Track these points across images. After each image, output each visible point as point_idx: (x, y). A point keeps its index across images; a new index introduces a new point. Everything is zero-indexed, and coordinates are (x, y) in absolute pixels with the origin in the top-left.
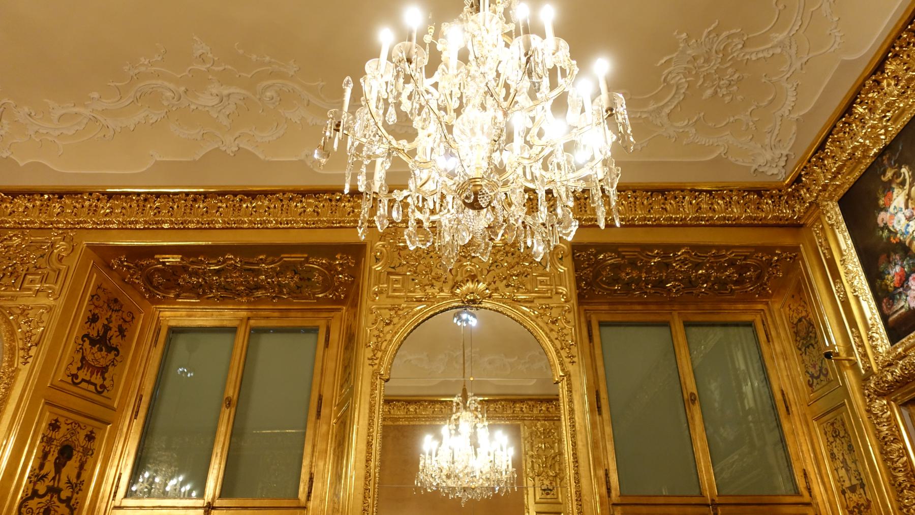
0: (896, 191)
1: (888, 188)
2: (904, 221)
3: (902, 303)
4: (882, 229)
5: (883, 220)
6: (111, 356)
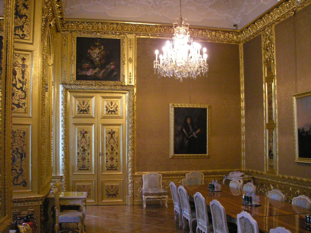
0: (97, 49)
1: (96, 46)
2: (96, 56)
3: (85, 72)
4: (88, 53)
5: (90, 52)
6: (24, 19)
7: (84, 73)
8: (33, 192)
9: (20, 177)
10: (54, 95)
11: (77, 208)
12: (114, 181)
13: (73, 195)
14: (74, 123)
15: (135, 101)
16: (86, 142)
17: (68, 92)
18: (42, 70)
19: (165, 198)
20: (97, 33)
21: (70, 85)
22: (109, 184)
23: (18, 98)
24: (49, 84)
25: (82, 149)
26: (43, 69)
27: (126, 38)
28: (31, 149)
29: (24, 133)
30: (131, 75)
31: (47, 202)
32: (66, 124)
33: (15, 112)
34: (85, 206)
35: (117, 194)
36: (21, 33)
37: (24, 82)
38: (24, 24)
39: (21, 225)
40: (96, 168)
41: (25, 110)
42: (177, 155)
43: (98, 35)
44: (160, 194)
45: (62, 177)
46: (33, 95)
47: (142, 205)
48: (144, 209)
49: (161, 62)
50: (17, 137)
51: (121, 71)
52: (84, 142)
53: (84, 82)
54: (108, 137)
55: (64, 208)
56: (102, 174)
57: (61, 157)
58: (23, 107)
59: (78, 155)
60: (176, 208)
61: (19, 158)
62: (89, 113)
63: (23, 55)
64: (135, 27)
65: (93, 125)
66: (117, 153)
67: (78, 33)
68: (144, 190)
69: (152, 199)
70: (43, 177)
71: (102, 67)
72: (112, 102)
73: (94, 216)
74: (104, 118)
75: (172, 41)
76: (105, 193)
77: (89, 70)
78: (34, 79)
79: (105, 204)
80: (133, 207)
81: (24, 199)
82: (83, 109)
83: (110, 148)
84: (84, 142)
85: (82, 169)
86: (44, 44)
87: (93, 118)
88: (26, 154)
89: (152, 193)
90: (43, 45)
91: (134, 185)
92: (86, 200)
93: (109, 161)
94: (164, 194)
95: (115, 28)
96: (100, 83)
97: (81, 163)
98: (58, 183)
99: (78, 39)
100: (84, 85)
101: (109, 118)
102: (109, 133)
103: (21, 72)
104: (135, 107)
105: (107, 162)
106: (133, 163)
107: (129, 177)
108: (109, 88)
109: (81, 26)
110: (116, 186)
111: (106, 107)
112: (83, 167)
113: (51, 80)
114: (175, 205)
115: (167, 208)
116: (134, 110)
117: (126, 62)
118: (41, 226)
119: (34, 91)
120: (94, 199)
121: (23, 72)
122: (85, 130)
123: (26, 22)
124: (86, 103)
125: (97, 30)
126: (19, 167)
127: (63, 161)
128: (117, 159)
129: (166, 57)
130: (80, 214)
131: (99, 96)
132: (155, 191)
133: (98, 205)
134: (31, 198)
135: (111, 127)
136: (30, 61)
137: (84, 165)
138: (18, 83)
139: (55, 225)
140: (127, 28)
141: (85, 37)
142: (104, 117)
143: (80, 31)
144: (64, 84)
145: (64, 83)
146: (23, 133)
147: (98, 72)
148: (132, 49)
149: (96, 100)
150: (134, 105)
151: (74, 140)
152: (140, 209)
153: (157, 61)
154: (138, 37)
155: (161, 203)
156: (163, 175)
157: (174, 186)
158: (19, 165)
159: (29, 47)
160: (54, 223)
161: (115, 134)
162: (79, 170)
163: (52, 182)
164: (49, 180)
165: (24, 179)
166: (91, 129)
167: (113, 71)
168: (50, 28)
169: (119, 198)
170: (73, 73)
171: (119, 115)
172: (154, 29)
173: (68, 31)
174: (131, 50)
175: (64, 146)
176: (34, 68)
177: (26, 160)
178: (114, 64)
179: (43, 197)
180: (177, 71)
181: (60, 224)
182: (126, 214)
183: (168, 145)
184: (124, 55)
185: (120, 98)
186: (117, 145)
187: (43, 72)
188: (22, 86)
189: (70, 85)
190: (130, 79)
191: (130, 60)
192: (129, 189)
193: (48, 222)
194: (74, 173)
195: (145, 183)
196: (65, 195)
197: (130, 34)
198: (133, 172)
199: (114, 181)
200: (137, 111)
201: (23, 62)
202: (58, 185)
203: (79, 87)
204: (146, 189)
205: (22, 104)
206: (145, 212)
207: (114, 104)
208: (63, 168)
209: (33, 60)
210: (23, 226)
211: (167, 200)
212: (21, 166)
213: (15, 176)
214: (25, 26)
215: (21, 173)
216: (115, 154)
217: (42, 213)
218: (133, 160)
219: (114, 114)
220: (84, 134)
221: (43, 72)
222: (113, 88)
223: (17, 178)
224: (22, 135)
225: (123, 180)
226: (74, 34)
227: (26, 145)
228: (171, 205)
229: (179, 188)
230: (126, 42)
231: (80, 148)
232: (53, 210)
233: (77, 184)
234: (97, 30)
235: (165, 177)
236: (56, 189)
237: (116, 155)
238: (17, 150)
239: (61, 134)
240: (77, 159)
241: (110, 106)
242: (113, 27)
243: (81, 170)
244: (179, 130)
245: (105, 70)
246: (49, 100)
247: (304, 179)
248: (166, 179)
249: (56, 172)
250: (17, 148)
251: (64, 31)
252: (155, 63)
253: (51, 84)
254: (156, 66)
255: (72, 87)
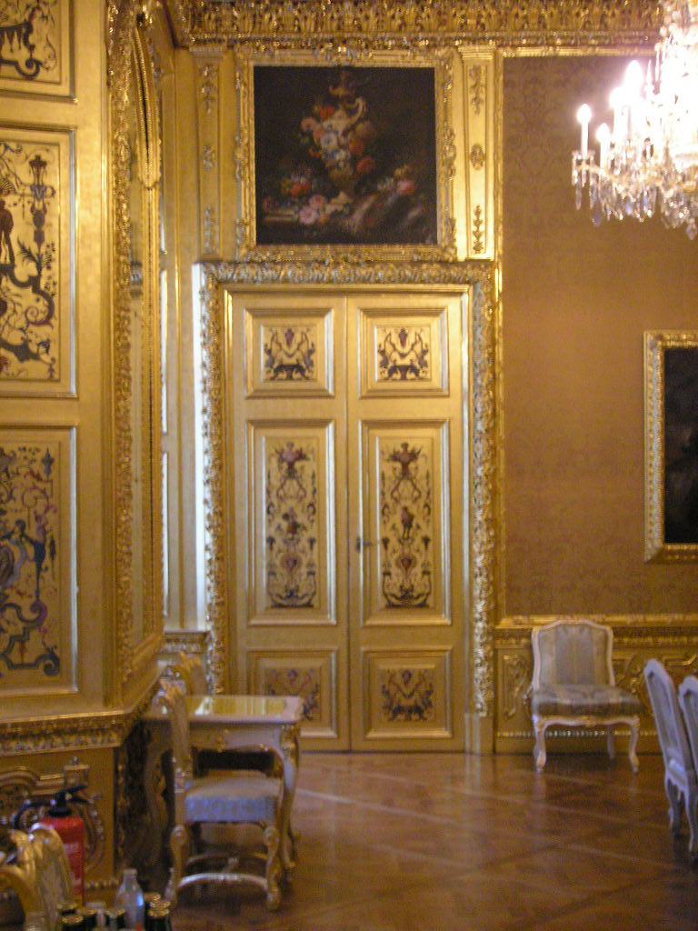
1: (333, 102)
2: (334, 143)
3: (292, 212)
4: (304, 134)
5: (308, 126)
7: (288, 214)
8: (83, 697)
9: (34, 634)
10: (171, 305)
11: (262, 762)
12: (417, 654)
13: (249, 710)
14: (252, 417)
15: (499, 323)
16: (301, 493)
17: (226, 293)
18: (113, 206)
19: (627, 726)
20: (335, 47)
21: (235, 264)
22: (395, 666)
23: (22, 323)
24: (145, 262)
25: (285, 525)
26: (119, 202)
27: (457, 59)
28: (78, 524)
29: (48, 461)
30: (482, 217)
31: (141, 741)
32: (220, 423)
33: (10, 379)
34: (296, 754)
35: (429, 704)
36: (22, 55)
37: (44, 257)
38: (32, 16)
39: (27, 833)
40: (344, 602)
41: (51, 370)
42: (676, 547)
43: (344, 55)
44: (605, 710)
45: (205, 634)
46: (81, 310)
47: (529, 755)
48: (539, 770)
49: (606, 156)
50: (21, 479)
51: (441, 200)
52: (292, 492)
53: (290, 251)
54: (389, 473)
55: (211, 763)
56: (368, 622)
57: (202, 558)
58: (44, 357)
59: (271, 548)
60: (673, 772)
61: (27, 562)
62: (314, 376)
63: (33, 147)
64: (494, 13)
65: (331, 426)
66: (426, 540)
67: (258, 48)
68: (538, 693)
69: (573, 728)
70: (127, 637)
71: (362, 186)
72: (403, 331)
73: (334, 798)
74: (373, 395)
75: (654, 64)
76: (379, 700)
77: (307, 204)
78: (82, 242)
79: (379, 746)
80: (494, 761)
81: (49, 723)
82: (287, 361)
83: (397, 519)
84: (292, 492)
85: (285, 603)
86: (117, 99)
87: (329, 397)
88: (57, 543)
89: (571, 706)
90: (116, 104)
91: (496, 669)
92: (298, 731)
93: (394, 570)
94: (623, 710)
95: (410, 20)
96: (354, 253)
97: (282, 579)
98: (189, 662)
99: (260, 72)
100: (291, 264)
101: (395, 395)
102: (395, 457)
103: (29, 216)
104: (500, 350)
105: (387, 574)
106: (492, 578)
107: (478, 639)
108: (389, 273)
109: (271, 19)
110: (423, 676)
111: (382, 352)
112: (292, 594)
113: (154, 247)
114: (669, 759)
115: (635, 770)
116: (494, 361)
117: (459, 164)
118: (116, 832)
119: (83, 289)
120: (334, 724)
121: (39, 218)
122: (297, 447)
123: (39, 8)
124: (298, 338)
125: (338, 34)
126: (30, 596)
127: (211, 573)
128: (429, 564)
129: (626, 132)
130: (272, 787)
131: (351, 306)
132: (585, 696)
133: (348, 752)
134: (75, 720)
135: (404, 433)
136: (65, 172)
137: (292, 586)
138: (18, 260)
139: (172, 831)
140: (463, 17)
141: (288, 63)
142: (369, 391)
143: (266, 40)
144: (208, 261)
145: (212, 257)
146: (43, 461)
147: (346, 211)
148: (482, 108)
149: (338, 322)
150: (493, 343)
151: (252, 490)
152: (523, 772)
153: (584, 153)
154: (506, 53)
155: (610, 749)
156: (620, 631)
157: (666, 679)
158: (32, 591)
159: (58, 114)
160: (171, 824)
161: (420, 461)
162: (272, 607)
163: (165, 654)
164: (150, 648)
165: (50, 644)
166: (321, 442)
167: (404, 203)
168: (143, 29)
169: (436, 724)
170: (243, 216)
171: (436, 383)
172: (578, 15)
173: (220, 41)
174: (478, 112)
175: (215, 513)
176: (83, 200)
177: (56, 570)
178: (408, 176)
179: (127, 717)
180: (668, 194)
181: (195, 828)
182: (466, 790)
183: (640, 504)
184: (452, 134)
185: (436, 312)
186: (426, 505)
187: (120, 216)
188: (34, 272)
189: (235, 264)
190: (477, 235)
191: (476, 156)
192: (477, 685)
193: (147, 819)
194: (253, 622)
195: (543, 665)
196: (218, 709)
197: (474, 41)
198: (493, 615)
199: (417, 654)
200: (507, 370)
201: (38, 175)
202: (188, 669)
203: (269, 273)
204: (546, 689)
205: (39, 345)
206: (541, 785)
207: (411, 339)
208: (209, 601)
209: (75, 165)
210: (32, 837)
211: (637, 735)
212: (38, 592)
213: (12, 630)
214: (36, 23)
215: (38, 622)
216: (418, 541)
217: (121, 780)
218: (492, 566)
219: (299, 380)
220: (292, 462)
221: (120, 216)
222: (406, 276)
223: (21, 639)
224: (38, 467)
225: (452, 651)
226: (242, 53)
227: (59, 510)
228: (653, 756)
229: (683, 689)
230: (458, 79)
231: (279, 520)
232: (167, 769)
233: (268, 663)
234: (338, 34)
235: (626, 640)
236: (180, 687)
237: (422, 547)
238: (23, 529)
239: (202, 461)
240: (265, 563)
241: (399, 347)
242: (402, 18)
243: (280, 606)
244: (687, 445)
245: (372, 199)
246: (151, 330)
247: (132, 13)
248: (634, 647)
249: (182, 611)
250: (19, 522)
251: (204, 42)
252: (579, 163)
253: (155, 261)
254: (584, 173)
255: (243, 274)
